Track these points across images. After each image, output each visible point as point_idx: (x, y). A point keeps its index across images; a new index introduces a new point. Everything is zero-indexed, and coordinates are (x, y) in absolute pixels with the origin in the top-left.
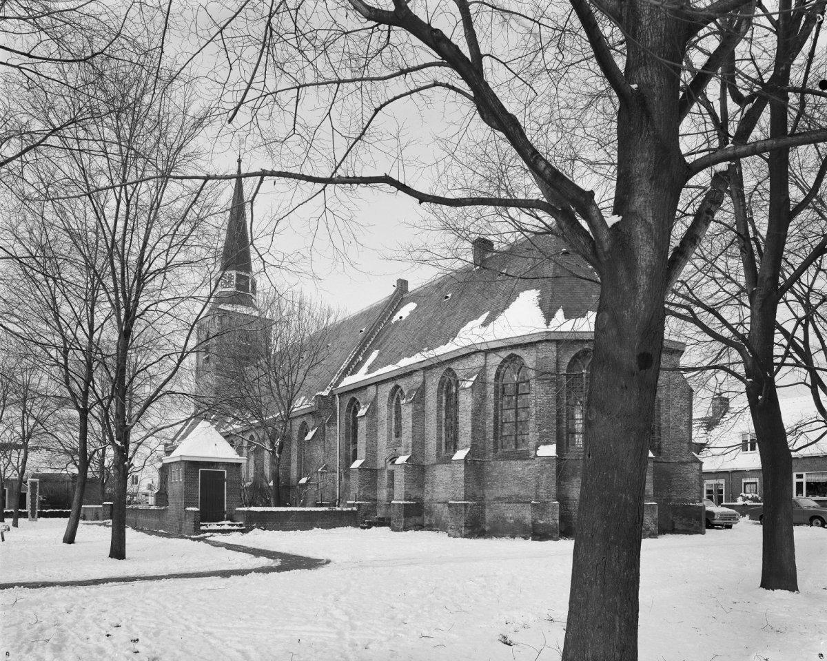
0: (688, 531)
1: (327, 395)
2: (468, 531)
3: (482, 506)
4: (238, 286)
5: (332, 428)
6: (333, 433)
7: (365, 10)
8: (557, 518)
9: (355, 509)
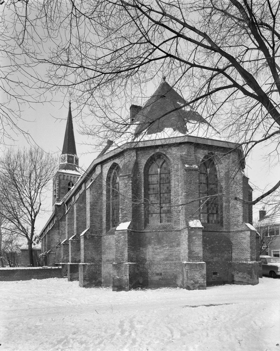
0: (242, 282)
1: (61, 204)
2: (86, 283)
3: (99, 266)
4: (68, 161)
5: (63, 222)
6: (64, 225)
7: (196, 31)
8: (128, 274)
9: (60, 267)
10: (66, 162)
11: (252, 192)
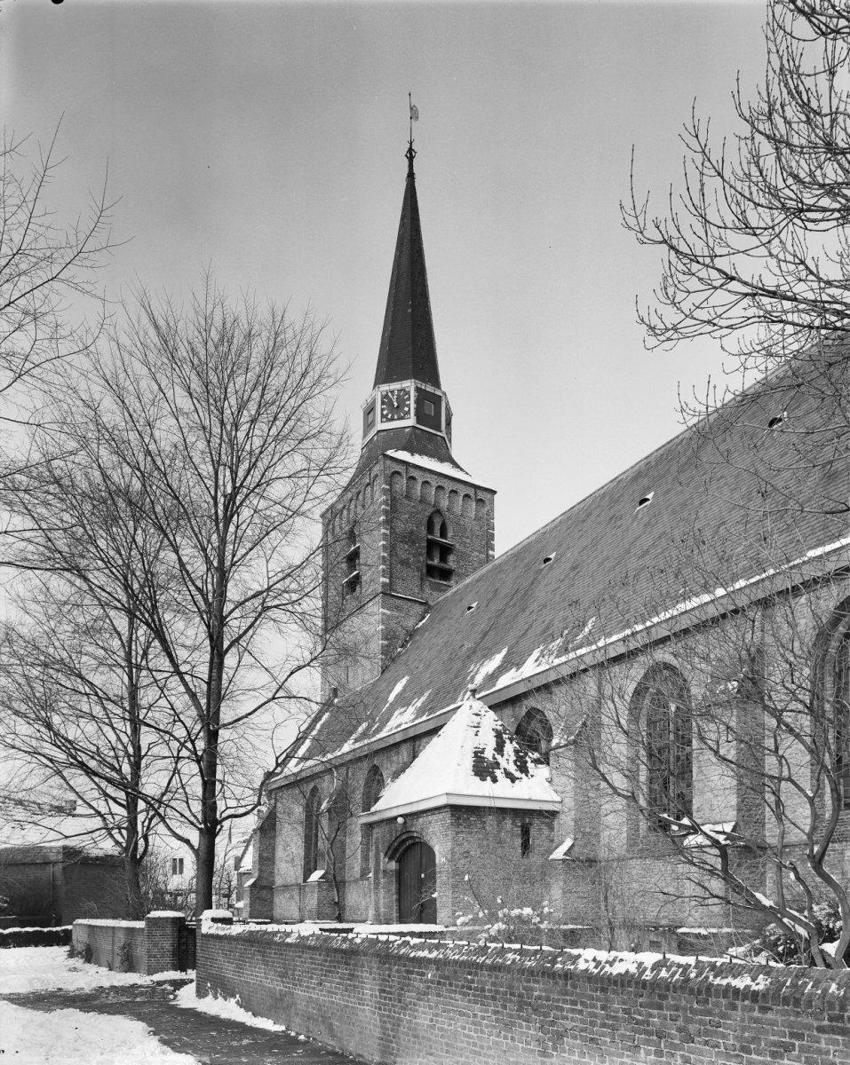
4: (420, 417)
10: (411, 421)
11: (64, 939)
